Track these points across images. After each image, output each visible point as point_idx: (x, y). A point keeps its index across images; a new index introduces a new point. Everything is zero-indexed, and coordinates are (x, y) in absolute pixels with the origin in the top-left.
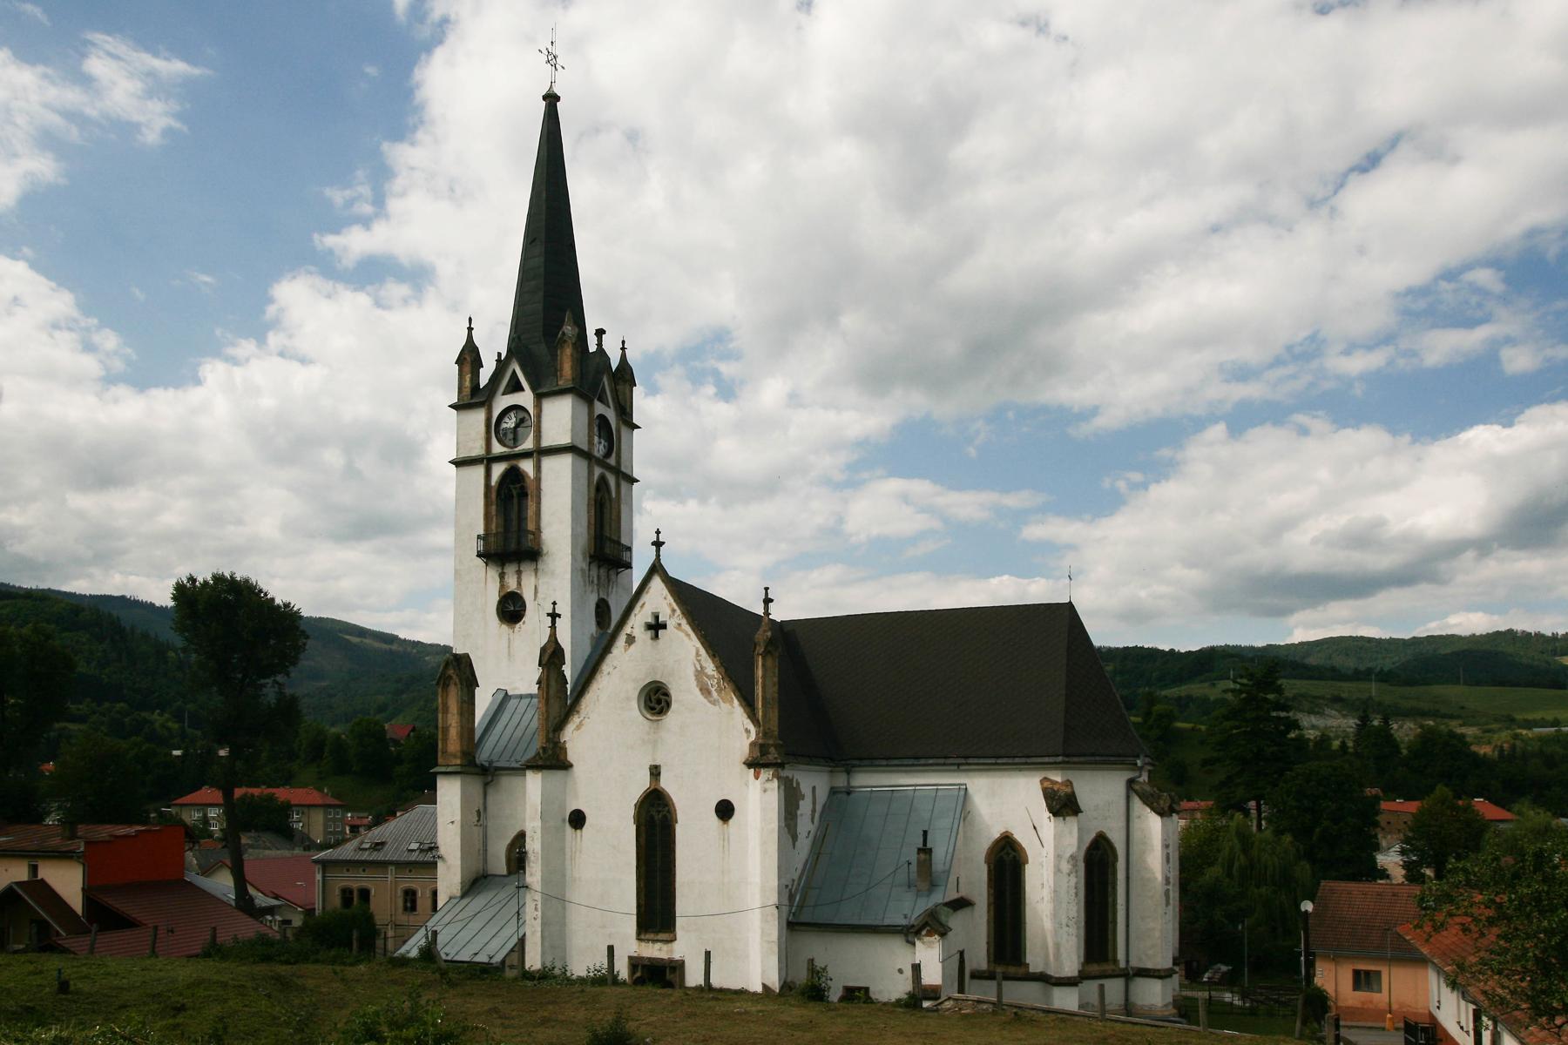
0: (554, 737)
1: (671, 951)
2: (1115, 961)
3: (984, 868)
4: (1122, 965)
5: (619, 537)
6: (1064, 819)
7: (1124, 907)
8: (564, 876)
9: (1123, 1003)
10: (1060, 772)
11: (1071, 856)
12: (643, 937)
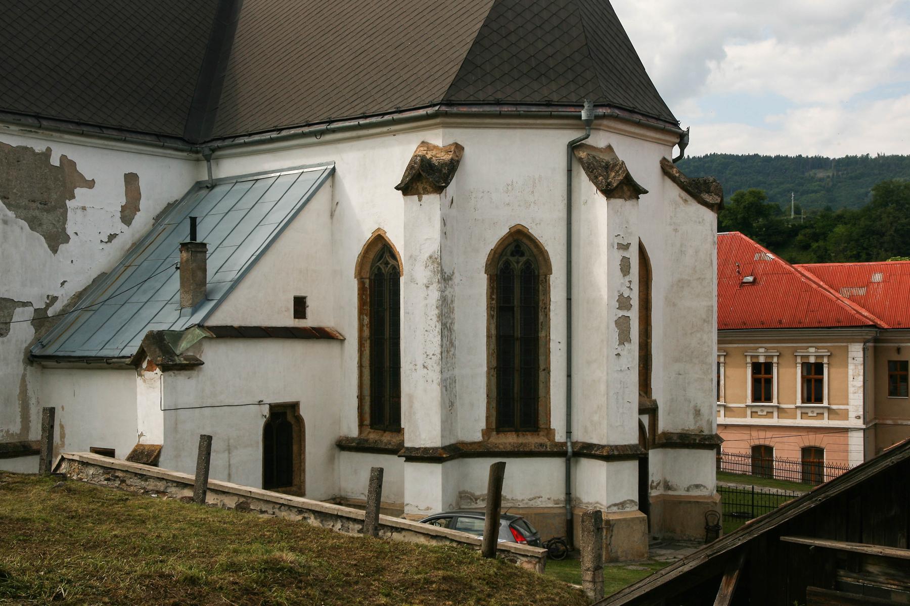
2: (550, 432)
3: (354, 284)
4: (560, 437)
6: (420, 200)
7: (563, 346)
9: (562, 497)
10: (440, 131)
11: (431, 257)
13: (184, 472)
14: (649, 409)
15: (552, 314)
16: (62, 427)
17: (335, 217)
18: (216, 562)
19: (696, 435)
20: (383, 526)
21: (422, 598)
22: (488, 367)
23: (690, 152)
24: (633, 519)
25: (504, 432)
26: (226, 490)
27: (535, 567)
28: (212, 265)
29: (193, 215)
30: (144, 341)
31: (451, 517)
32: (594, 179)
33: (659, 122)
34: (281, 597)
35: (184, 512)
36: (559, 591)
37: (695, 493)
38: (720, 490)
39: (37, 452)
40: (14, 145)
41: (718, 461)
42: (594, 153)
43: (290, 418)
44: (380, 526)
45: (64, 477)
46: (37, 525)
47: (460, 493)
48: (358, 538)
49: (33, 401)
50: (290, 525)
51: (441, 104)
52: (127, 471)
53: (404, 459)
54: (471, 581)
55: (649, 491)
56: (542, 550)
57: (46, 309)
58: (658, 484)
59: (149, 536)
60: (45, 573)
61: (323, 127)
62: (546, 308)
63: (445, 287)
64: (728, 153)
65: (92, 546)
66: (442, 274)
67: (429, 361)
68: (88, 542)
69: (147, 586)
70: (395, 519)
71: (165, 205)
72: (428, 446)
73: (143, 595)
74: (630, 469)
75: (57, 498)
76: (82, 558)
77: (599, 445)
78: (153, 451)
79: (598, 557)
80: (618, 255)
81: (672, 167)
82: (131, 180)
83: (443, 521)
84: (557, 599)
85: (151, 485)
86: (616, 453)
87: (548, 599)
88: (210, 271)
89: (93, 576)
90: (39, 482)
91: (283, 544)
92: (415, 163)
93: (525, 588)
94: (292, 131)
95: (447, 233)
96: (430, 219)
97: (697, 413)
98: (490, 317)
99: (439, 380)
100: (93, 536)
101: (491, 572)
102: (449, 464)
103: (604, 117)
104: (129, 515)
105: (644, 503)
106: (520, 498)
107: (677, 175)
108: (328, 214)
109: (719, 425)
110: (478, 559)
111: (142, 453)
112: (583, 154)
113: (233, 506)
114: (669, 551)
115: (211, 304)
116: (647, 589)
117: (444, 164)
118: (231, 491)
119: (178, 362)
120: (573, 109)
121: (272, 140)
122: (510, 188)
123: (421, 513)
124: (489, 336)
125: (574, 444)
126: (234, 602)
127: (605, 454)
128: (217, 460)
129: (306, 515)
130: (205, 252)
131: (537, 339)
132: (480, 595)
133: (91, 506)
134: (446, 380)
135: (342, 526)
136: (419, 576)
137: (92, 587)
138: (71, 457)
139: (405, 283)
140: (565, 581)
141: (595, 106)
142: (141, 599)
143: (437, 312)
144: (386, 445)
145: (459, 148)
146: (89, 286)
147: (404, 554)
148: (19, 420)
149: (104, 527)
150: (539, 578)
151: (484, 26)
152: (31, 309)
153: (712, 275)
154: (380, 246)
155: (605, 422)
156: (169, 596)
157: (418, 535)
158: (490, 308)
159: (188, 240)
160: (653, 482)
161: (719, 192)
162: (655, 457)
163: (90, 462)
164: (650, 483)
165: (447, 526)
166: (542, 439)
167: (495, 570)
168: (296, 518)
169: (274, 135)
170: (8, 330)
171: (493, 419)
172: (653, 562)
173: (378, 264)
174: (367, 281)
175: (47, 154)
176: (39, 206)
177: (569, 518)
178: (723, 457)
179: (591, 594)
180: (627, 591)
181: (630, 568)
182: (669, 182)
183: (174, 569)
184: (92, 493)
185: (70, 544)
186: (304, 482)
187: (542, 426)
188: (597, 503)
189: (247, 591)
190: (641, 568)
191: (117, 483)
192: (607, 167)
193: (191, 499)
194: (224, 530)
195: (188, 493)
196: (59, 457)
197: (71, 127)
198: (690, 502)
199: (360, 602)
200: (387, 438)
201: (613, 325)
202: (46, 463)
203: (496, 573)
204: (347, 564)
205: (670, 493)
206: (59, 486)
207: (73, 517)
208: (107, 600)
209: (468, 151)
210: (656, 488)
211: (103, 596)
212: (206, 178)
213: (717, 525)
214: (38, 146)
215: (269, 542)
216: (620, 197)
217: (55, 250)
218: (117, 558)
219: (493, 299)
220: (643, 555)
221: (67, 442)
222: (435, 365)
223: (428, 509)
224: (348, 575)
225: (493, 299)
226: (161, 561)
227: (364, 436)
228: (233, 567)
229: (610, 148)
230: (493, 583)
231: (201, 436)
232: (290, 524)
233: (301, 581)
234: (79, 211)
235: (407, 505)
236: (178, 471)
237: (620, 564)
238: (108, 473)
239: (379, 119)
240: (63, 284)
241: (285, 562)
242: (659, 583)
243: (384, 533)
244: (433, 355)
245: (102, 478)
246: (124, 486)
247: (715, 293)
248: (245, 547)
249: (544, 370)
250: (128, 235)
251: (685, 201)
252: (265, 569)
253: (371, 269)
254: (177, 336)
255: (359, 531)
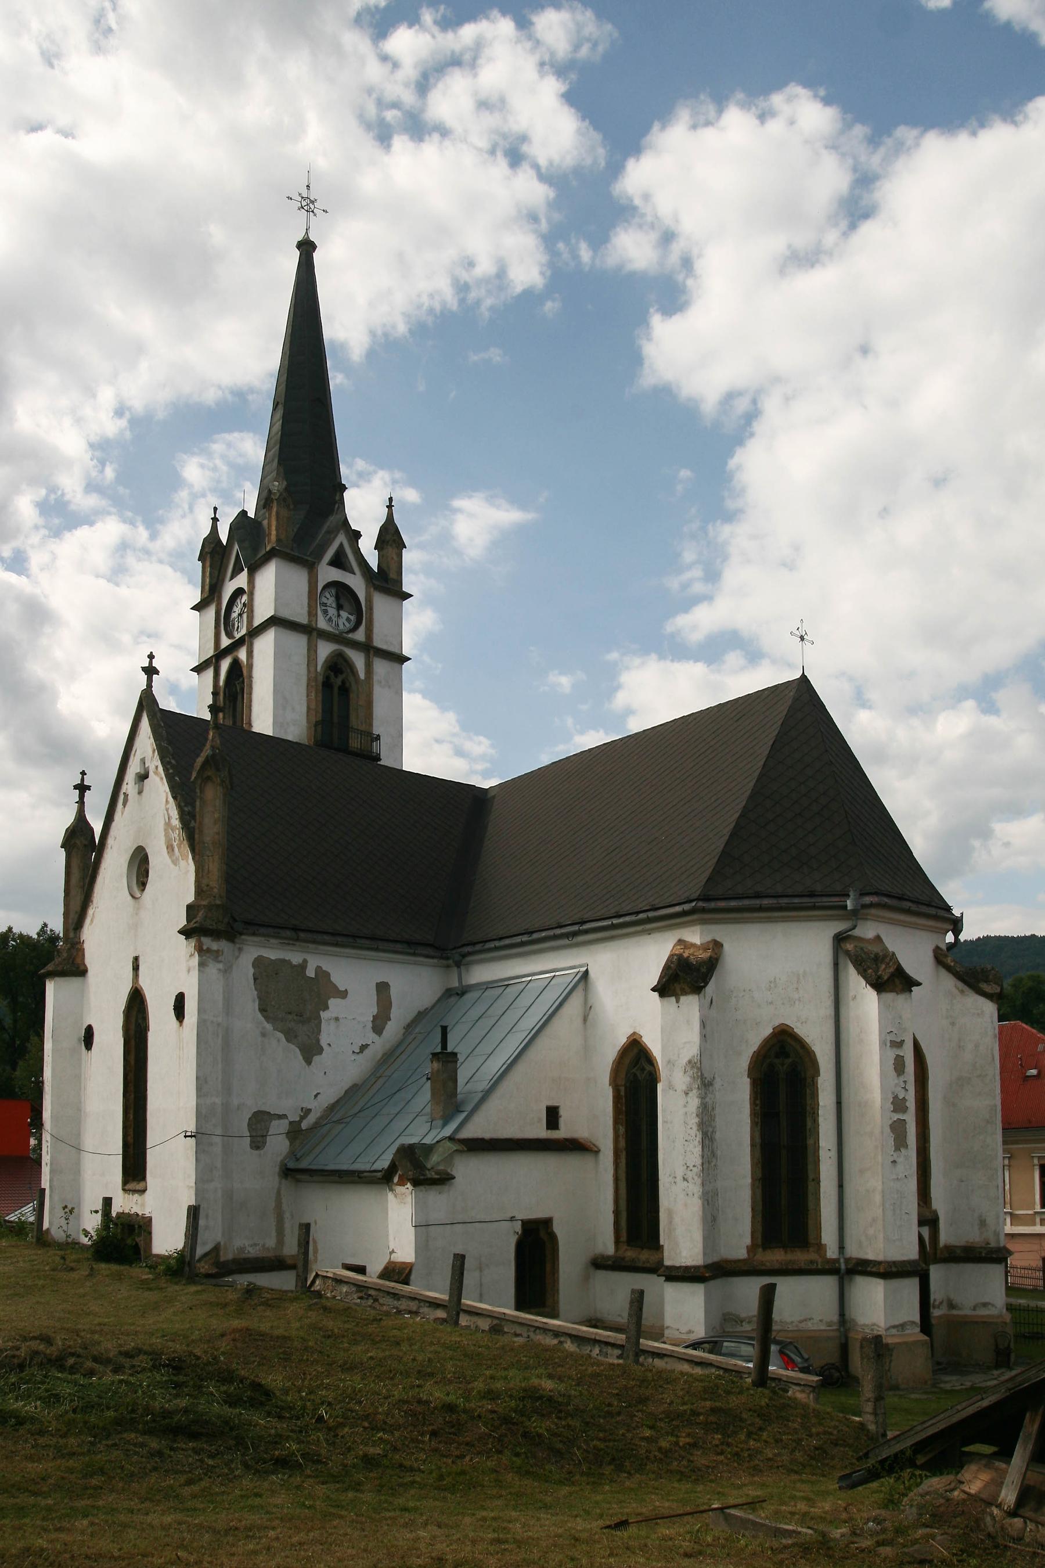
0: (76, 937)
1: (143, 1205)
2: (820, 1247)
3: (609, 1093)
4: (832, 1253)
5: (371, 725)
6: (678, 1001)
7: (834, 1154)
8: (79, 1110)
9: (835, 1318)
10: (697, 928)
11: (690, 1062)
12: (128, 1187)
13: (436, 1291)
14: (929, 1220)
15: (821, 1120)
16: (315, 1242)
17: (588, 1023)
18: (473, 1388)
19: (981, 1248)
20: (645, 1352)
21: (688, 1430)
22: (752, 1178)
23: (962, 937)
24: (916, 1342)
25: (770, 1248)
26: (479, 1312)
27: (809, 1397)
28: (463, 1075)
29: (444, 1024)
30: (395, 1155)
31: (716, 1342)
32: (863, 972)
33: (930, 908)
34: (541, 1427)
35: (438, 1334)
36: (837, 1424)
37: (983, 1312)
38: (1010, 1308)
39: (293, 1267)
40: (273, 958)
41: (1007, 1272)
42: (862, 945)
43: (542, 1234)
44: (641, 1352)
45: (318, 1294)
46: (296, 1343)
47: (724, 1314)
48: (619, 1365)
49: (287, 1215)
50: (547, 1350)
51: (697, 899)
52: (379, 1290)
53: (664, 1278)
54: (741, 1413)
55: (932, 1310)
56: (816, 1378)
57: (300, 1122)
58: (941, 1303)
59: (405, 1359)
60: (307, 1394)
61: (576, 928)
62: (814, 1113)
63: (706, 1093)
64: (1002, 935)
65: (349, 1367)
66: (702, 1079)
67: (689, 1173)
68: (346, 1363)
69: (406, 1413)
70: (656, 1344)
71: (416, 1012)
72: (689, 1264)
73: (401, 1421)
74: (910, 1288)
75: (313, 1316)
76: (340, 1380)
77: (875, 1261)
78: (404, 1269)
79: (879, 1387)
80: (891, 1054)
81: (946, 956)
82: (383, 988)
83: (706, 1345)
84: (835, 1432)
85: (403, 1304)
86: (894, 1269)
87: (825, 1433)
88: (461, 1080)
89: (352, 1399)
90: (296, 1299)
91: (541, 1371)
92: (672, 962)
93: (799, 1420)
94: (543, 934)
95: (707, 1036)
96: (688, 1021)
97: (983, 1223)
98: (754, 1124)
99: (700, 1193)
100: (349, 1357)
101: (763, 1403)
102: (712, 1283)
103: (871, 905)
104: (383, 1336)
105: (926, 1324)
106: (789, 1320)
107: (952, 964)
108: (580, 1020)
109: (1007, 1235)
110: (748, 1389)
111: (394, 1270)
112: (849, 946)
113: (487, 1328)
114: (954, 1378)
115: (462, 1117)
116: (942, 1426)
117: (702, 963)
118: (484, 1313)
119: (429, 1176)
120: (837, 899)
121: (522, 944)
122: (772, 985)
123: (684, 1337)
124: (753, 1145)
125: (847, 1260)
126: (493, 1431)
127: (882, 1271)
128: (470, 1279)
129: (562, 1339)
130: (456, 1062)
131: (805, 1147)
132: (751, 1428)
133: (347, 1326)
134: (707, 1193)
135: (600, 1351)
136: (685, 1407)
137: (352, 1411)
138: (325, 1274)
139: (663, 1090)
140: (842, 1412)
141: (861, 894)
142: (399, 1425)
143: (697, 1120)
144: (644, 1263)
145: (717, 945)
146: (341, 1098)
147: (668, 1383)
148: (274, 1234)
149: (360, 1348)
150: (814, 1410)
151: (741, 816)
152: (286, 1122)
153: (994, 1070)
154: (635, 1051)
155: (881, 1235)
156: (427, 1423)
157: (681, 1361)
158: (753, 1114)
159: (439, 1050)
160: (935, 1300)
161: (998, 982)
162: (936, 1273)
163: (344, 1279)
164: (932, 1301)
165: (711, 1352)
166: (813, 1256)
167: (767, 1400)
168: (551, 1341)
169: (525, 938)
170: (265, 1143)
171: (759, 1235)
172: (936, 1390)
173: (634, 1070)
174: (622, 1089)
175: (303, 966)
176: (295, 1018)
177: (843, 1341)
178: (1012, 1271)
179: (872, 1427)
180: (919, 1428)
181: (913, 1396)
182: (943, 973)
183: (431, 1394)
184: (347, 1311)
185: (328, 1364)
186: (558, 1302)
187: (812, 1241)
188: (874, 1325)
189: (506, 1420)
190: (925, 1397)
191: (370, 1302)
192: (877, 959)
193: (444, 1321)
194: (479, 1354)
195: (441, 1314)
196: (314, 1274)
197: (326, 938)
198: (976, 1323)
199: (623, 1435)
200: (645, 1256)
201: (888, 1130)
202: (302, 1279)
203: (768, 1405)
204: (609, 1394)
205: (955, 1312)
206: (316, 1304)
207: (329, 1337)
208: (366, 1424)
209: (726, 947)
210: (939, 1307)
211: (363, 1420)
212: (456, 984)
213: (1008, 1348)
214: (295, 957)
215: (526, 1368)
216: (891, 991)
217: (308, 1061)
218: (374, 1381)
219: (756, 1105)
220: (926, 1383)
221: (319, 1258)
222: (696, 1178)
223: (690, 1332)
224: (610, 1405)
225: (756, 1105)
226: (418, 1386)
227: (620, 1253)
228: (490, 1395)
229: (878, 938)
230: (764, 1415)
231: (455, 1255)
232: (547, 1349)
233: (560, 1411)
234: (332, 1022)
235: (668, 1327)
236: (430, 1290)
237: (901, 1393)
238: (361, 1291)
239: (633, 918)
240: (316, 1096)
241: (544, 1390)
242: (955, 1420)
243: (645, 1359)
244: (694, 1166)
245: (355, 1296)
246: (376, 1305)
247: (998, 1091)
248: (504, 1373)
249: (813, 1180)
250: (379, 1045)
251: (962, 992)
252: (524, 1398)
253: (626, 1075)
254: (429, 1149)
255: (619, 1357)
